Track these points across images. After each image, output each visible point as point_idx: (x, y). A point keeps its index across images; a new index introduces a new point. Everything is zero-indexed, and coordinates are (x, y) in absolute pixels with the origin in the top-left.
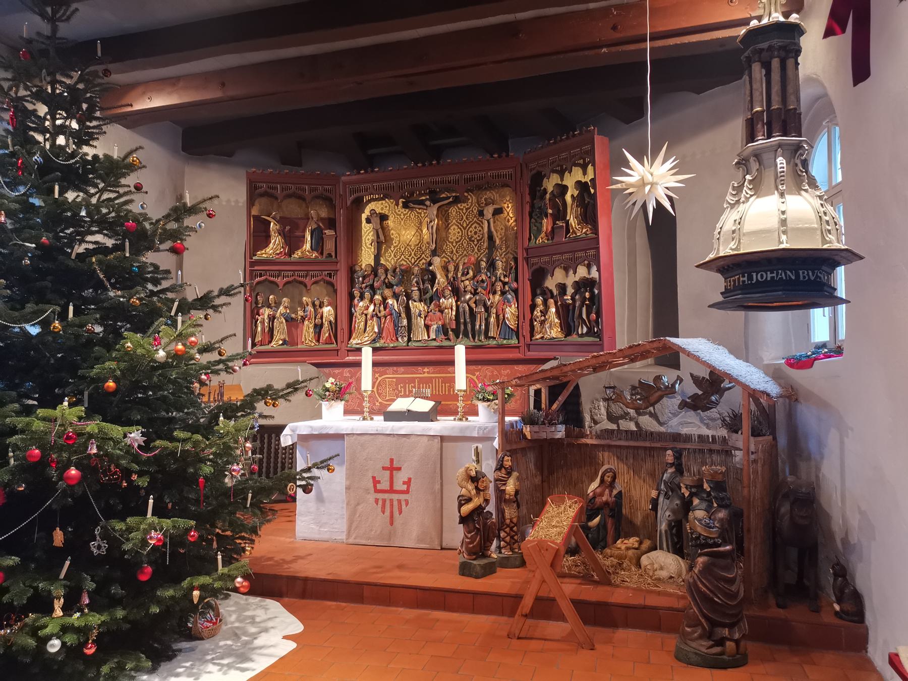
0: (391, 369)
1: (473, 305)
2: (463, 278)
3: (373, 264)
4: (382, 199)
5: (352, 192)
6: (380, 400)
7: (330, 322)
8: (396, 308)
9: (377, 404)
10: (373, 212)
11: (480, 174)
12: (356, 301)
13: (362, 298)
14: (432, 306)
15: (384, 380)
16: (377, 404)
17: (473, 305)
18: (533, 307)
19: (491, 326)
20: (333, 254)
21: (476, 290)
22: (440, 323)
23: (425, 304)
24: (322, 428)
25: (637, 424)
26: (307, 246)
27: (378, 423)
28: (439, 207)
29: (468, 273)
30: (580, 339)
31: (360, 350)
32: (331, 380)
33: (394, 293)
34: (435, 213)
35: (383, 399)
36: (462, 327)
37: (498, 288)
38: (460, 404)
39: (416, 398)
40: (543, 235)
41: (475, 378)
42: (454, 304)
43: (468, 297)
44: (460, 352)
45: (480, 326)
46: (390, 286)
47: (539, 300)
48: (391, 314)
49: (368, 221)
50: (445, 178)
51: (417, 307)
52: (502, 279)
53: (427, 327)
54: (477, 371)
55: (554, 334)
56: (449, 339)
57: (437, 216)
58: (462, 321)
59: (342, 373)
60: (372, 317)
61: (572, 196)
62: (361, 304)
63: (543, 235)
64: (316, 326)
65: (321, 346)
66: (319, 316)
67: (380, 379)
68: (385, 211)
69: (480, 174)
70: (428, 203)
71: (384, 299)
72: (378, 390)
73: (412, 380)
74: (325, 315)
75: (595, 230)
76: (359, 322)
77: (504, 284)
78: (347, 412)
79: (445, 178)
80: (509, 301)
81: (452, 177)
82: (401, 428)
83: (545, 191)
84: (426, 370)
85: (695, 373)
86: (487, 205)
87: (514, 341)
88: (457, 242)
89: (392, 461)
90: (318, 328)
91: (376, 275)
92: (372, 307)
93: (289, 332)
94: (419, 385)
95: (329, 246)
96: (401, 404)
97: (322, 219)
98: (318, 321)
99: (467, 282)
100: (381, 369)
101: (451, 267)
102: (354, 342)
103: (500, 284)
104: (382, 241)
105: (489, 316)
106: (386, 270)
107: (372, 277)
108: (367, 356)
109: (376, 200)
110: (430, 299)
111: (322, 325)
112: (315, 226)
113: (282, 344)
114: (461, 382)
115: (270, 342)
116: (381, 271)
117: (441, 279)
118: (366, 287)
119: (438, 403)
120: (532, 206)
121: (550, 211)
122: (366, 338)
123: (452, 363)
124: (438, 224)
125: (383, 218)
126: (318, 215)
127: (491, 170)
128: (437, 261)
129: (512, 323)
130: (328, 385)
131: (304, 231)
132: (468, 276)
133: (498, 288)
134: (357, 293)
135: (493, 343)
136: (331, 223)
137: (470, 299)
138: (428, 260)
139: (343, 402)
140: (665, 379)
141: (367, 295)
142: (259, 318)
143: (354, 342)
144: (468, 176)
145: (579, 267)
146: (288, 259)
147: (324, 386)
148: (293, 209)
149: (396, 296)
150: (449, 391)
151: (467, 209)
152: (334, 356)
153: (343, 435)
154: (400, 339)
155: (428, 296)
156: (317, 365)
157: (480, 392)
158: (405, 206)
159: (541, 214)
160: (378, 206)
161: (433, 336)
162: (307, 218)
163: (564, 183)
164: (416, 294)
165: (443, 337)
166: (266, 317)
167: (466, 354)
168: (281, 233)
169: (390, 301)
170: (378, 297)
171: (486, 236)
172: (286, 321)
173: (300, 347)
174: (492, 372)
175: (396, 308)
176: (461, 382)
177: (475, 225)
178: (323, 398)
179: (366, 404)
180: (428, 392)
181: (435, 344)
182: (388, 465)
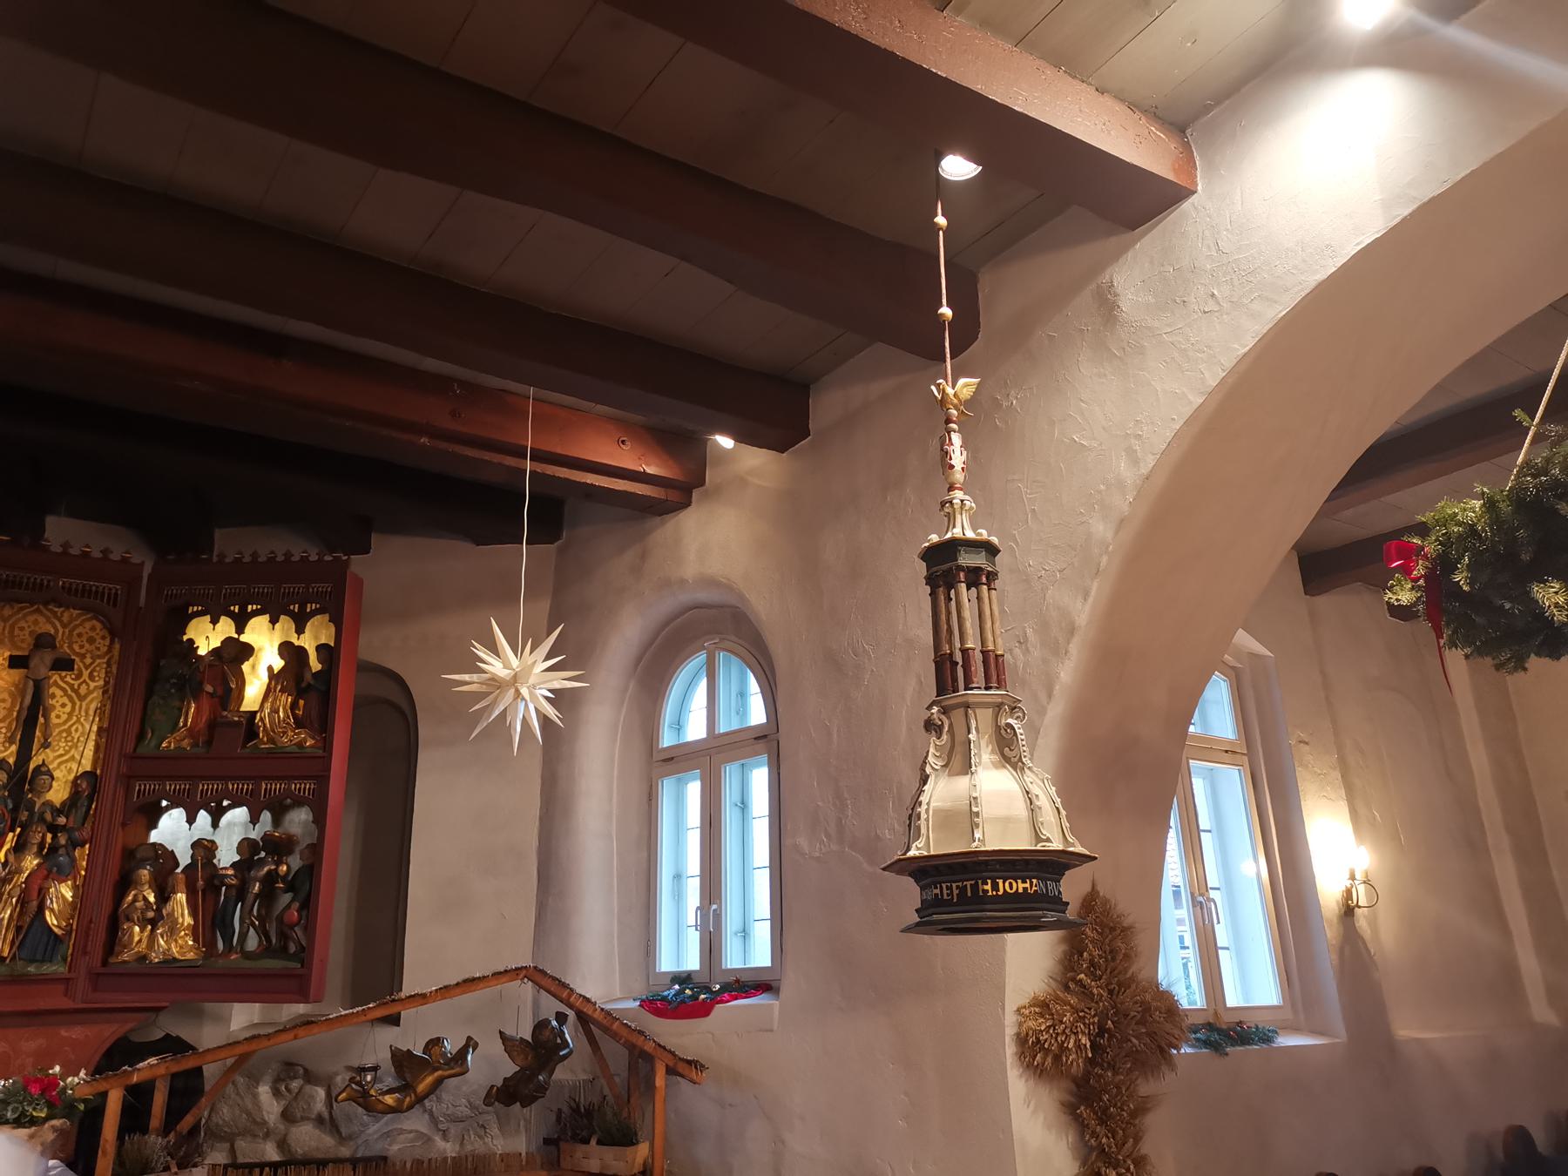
18: (125, 882)
25: (282, 1145)
30: (248, 964)
52: (48, 817)
75: (326, 745)
85: (509, 1032)
87: (56, 968)
121: (209, 688)
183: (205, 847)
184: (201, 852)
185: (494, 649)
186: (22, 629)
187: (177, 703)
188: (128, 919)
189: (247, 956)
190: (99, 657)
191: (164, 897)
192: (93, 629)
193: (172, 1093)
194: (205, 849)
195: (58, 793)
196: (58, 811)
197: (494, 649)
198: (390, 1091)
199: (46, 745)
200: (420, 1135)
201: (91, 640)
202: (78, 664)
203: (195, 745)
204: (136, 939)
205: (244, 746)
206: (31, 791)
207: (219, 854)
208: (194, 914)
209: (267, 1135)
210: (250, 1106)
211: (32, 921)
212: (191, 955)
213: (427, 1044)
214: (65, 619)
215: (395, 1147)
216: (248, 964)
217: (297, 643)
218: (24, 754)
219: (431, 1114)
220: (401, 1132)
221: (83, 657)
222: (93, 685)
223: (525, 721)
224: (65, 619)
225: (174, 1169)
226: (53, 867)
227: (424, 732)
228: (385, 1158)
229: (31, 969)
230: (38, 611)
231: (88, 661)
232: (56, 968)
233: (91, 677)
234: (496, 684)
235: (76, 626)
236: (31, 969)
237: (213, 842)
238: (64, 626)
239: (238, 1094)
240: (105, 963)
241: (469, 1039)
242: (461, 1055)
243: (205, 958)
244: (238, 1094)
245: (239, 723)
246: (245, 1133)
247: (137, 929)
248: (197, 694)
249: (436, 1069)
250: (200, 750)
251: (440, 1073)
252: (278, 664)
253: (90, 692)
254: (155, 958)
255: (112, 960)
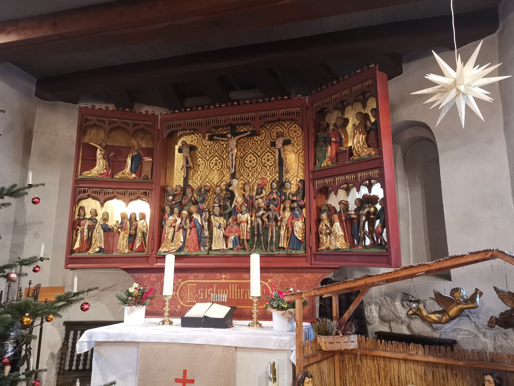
0: (192, 275)
1: (266, 220)
2: (257, 197)
3: (182, 185)
4: (193, 134)
5: (168, 127)
6: (182, 303)
7: (143, 232)
8: (199, 221)
9: (179, 307)
10: (184, 143)
11: (272, 112)
12: (166, 216)
13: (172, 213)
14: (231, 220)
15: (185, 285)
16: (179, 307)
17: (266, 220)
18: (319, 220)
19: (282, 238)
20: (149, 176)
21: (268, 206)
22: (237, 234)
23: (225, 218)
24: (118, 335)
25: (409, 327)
26: (128, 170)
27: (174, 332)
28: (239, 139)
29: (261, 193)
30: (365, 250)
31: (164, 257)
32: (136, 285)
33: (199, 209)
34: (235, 143)
35: (184, 302)
36: (258, 238)
37: (288, 205)
38: (255, 311)
39: (213, 302)
40: (327, 159)
41: (267, 284)
42: (249, 218)
43: (261, 213)
44: (255, 260)
45: (272, 237)
46: (196, 203)
47: (324, 216)
48: (196, 226)
49: (180, 151)
50: (244, 115)
51: (218, 221)
52: (291, 197)
53: (226, 238)
54: (271, 277)
55: (338, 245)
56: (244, 249)
57: (237, 146)
58: (256, 233)
59: (149, 278)
60: (179, 229)
61: (354, 125)
62: (171, 218)
63: (327, 159)
64: (130, 235)
65: (134, 254)
66: (133, 228)
67: (182, 283)
68: (195, 143)
69: (272, 112)
70: (229, 136)
71: (190, 214)
72: (180, 293)
73: (211, 285)
74: (139, 227)
75: (380, 152)
76: (169, 231)
77: (293, 202)
78: (149, 314)
79: (244, 115)
80: (296, 217)
81: (250, 115)
82: (196, 337)
83: (328, 125)
84: (223, 276)
85: (500, 288)
86: (278, 137)
87: (301, 252)
88: (252, 168)
89: (185, 372)
90: (132, 237)
91: (184, 194)
92: (179, 221)
93: (106, 242)
94: (217, 289)
95: (146, 170)
96: (198, 310)
97: (142, 149)
98: (133, 232)
99: (260, 201)
100: (184, 275)
101: (247, 188)
102: (162, 250)
103: (289, 201)
104: (189, 168)
105: (280, 228)
106: (193, 190)
107: (181, 195)
108: (170, 263)
109: (186, 135)
110: (229, 213)
111: (136, 234)
112: (135, 153)
113: (98, 252)
114: (255, 290)
115: (88, 249)
116: (188, 191)
117: (239, 199)
118: (176, 203)
119: (233, 308)
120: (316, 137)
121: (334, 139)
122: (174, 247)
123: (248, 270)
124: (237, 154)
125: (192, 148)
126: (139, 145)
127: (281, 109)
128: (235, 182)
129: (299, 235)
130: (131, 290)
131: (126, 158)
132: (262, 195)
133: (288, 205)
134: (168, 209)
135: (281, 252)
136: (149, 152)
137: (263, 214)
138: (228, 182)
139: (145, 307)
140: (464, 293)
141: (176, 210)
142: (80, 228)
143: (163, 250)
144: (263, 113)
145: (362, 187)
146: (109, 179)
147: (128, 291)
148: (119, 140)
149: (200, 212)
150: (244, 295)
151: (261, 141)
152: (140, 262)
153: (139, 343)
154: (202, 249)
155: (228, 211)
156: (127, 270)
157: (274, 300)
158: (211, 139)
159: (325, 143)
160: (189, 139)
161: (230, 246)
162: (129, 149)
163: (346, 116)
164: (217, 210)
165: (239, 246)
166: (86, 227)
167: (261, 262)
168: (106, 157)
169: (195, 216)
170: (185, 212)
171: (277, 161)
172: (104, 231)
173: (115, 254)
174: (283, 279)
175: (199, 221)
176: (255, 290)
177: (268, 153)
178: (125, 302)
179: (167, 309)
180: (224, 297)
181: (231, 253)
182: (181, 377)
183: (344, 204)
184: (342, 206)
185: (440, 73)
186: (273, 132)
187: (325, 148)
188: (322, 233)
189: (365, 247)
190: (299, 137)
191: (332, 223)
192: (295, 127)
193: (340, 301)
194: (345, 205)
195: (294, 189)
196: (293, 195)
197: (440, 73)
198: (435, 313)
199: (287, 172)
200: (471, 333)
201: (295, 132)
202: (293, 141)
203: (332, 163)
204: (325, 241)
205: (349, 160)
206: (285, 189)
207: (350, 206)
208: (344, 230)
209: (402, 323)
210: (393, 310)
211: (291, 234)
212: (344, 247)
213: (452, 290)
214: (286, 126)
215: (460, 337)
216: (365, 250)
217: (364, 112)
218: (281, 176)
219: (475, 323)
220: (461, 330)
221: (293, 138)
222: (298, 148)
223: (467, 108)
224: (286, 126)
225: (341, 335)
226: (294, 217)
227: (440, 146)
228: (455, 342)
229: (293, 252)
230: (277, 125)
231: (295, 139)
232: (301, 252)
233: (297, 145)
234: (445, 90)
235: (290, 128)
236: (293, 252)
237: (347, 202)
238: (286, 128)
239: (388, 304)
240: (317, 251)
241: (477, 290)
242: (473, 299)
243: (350, 248)
244: (388, 304)
245: (346, 150)
246: (393, 320)
247: (325, 237)
248: (330, 143)
249: (458, 304)
250: (334, 165)
251: (460, 306)
252: (357, 122)
253: (298, 151)
254: (332, 248)
255: (319, 249)
